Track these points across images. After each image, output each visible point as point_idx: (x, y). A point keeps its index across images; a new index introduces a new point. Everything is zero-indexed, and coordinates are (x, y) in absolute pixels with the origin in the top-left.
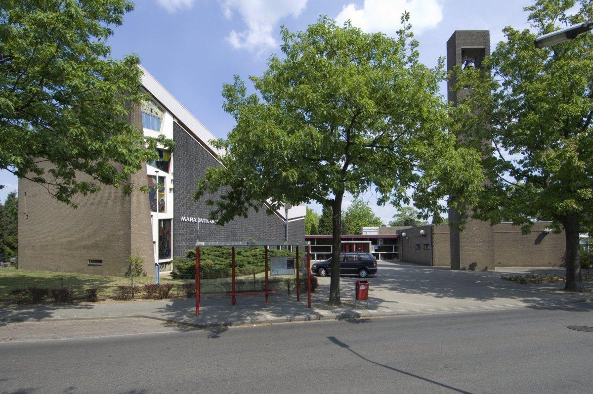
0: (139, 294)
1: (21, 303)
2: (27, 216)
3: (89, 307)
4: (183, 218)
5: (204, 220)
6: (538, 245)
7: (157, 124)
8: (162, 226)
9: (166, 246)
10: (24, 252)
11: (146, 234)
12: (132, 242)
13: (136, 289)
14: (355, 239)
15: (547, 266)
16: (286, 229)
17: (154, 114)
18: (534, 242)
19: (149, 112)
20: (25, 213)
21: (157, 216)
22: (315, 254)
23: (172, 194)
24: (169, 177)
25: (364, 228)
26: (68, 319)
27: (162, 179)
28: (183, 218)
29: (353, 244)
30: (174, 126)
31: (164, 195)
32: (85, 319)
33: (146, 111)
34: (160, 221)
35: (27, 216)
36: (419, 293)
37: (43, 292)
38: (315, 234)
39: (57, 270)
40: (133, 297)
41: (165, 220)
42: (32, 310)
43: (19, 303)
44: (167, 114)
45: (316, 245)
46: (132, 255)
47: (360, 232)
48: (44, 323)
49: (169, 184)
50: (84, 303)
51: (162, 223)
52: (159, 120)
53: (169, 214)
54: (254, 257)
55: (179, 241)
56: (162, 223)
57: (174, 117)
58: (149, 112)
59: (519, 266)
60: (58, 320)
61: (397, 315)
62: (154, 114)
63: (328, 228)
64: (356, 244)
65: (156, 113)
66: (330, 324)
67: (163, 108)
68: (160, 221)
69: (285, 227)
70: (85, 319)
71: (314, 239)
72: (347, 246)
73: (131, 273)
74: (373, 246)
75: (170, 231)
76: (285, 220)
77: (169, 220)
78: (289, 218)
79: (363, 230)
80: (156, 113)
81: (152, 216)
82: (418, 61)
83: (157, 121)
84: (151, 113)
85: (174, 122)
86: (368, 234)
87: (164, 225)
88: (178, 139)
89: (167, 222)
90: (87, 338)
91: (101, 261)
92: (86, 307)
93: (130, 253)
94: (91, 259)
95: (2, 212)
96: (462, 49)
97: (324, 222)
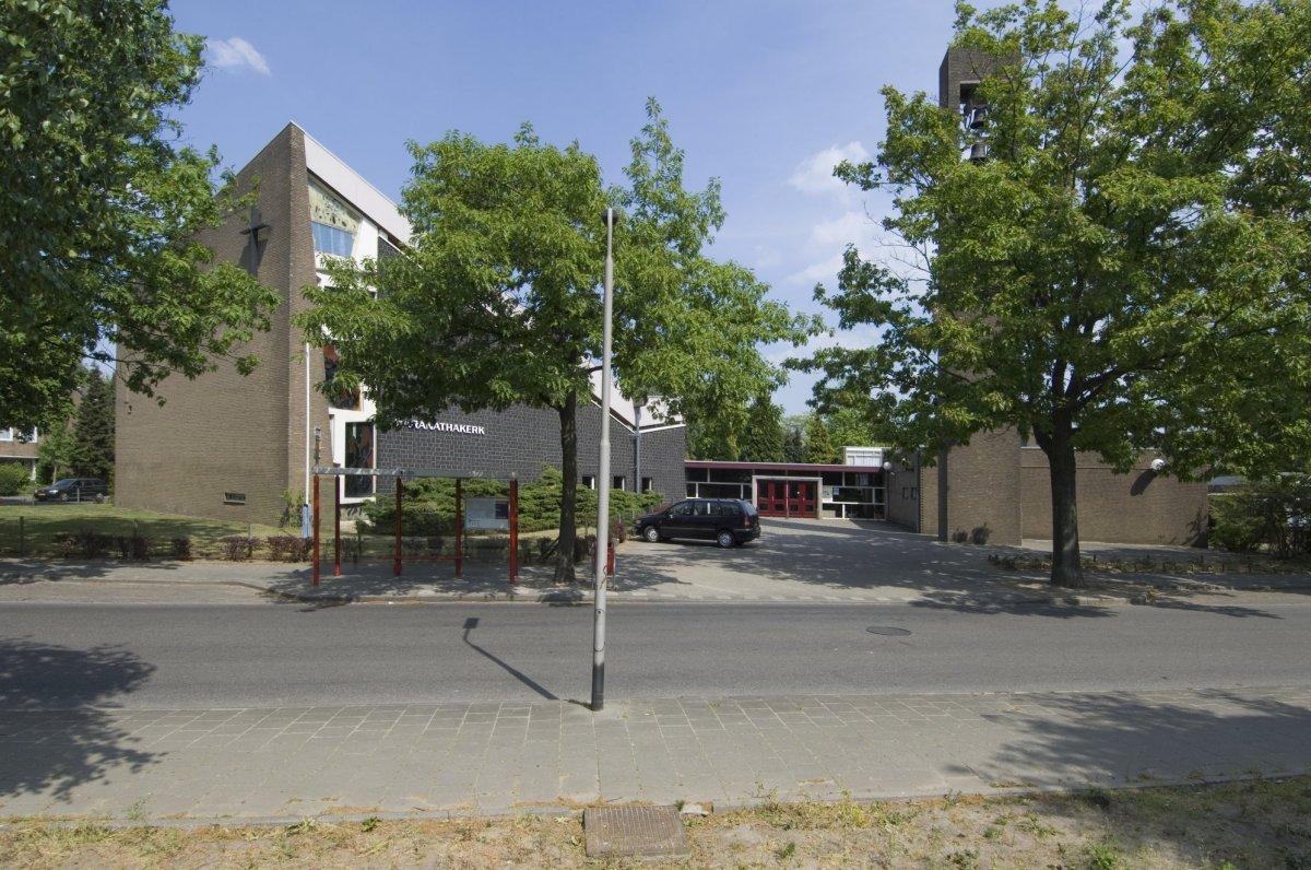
0: (260, 552)
1: (69, 556)
2: (130, 407)
6: (1138, 497)
8: (354, 435)
10: (124, 476)
12: (291, 463)
13: (253, 544)
14: (792, 473)
15: (1154, 542)
16: (635, 447)
17: (339, 224)
18: (1129, 490)
19: (329, 222)
20: (126, 403)
25: (848, 449)
26: (124, 581)
29: (784, 482)
32: (149, 582)
33: (322, 221)
34: (349, 426)
35: (130, 407)
36: (839, 587)
37: (106, 542)
38: (728, 459)
39: (176, 511)
40: (249, 556)
41: (359, 425)
42: (83, 567)
43: (67, 556)
44: (365, 224)
45: (697, 483)
46: (290, 487)
47: (839, 457)
48: (91, 584)
50: (166, 563)
51: (354, 429)
52: (350, 235)
54: (538, 502)
56: (354, 429)
57: (380, 228)
58: (329, 222)
59: (1098, 540)
60: (110, 581)
61: (650, 601)
62: (339, 224)
63: (762, 447)
64: (794, 485)
65: (344, 224)
66: (535, 607)
67: (357, 214)
68: (349, 426)
69: (635, 442)
70: (149, 582)
72: (772, 488)
73: (288, 519)
74: (830, 489)
75: (370, 444)
76: (635, 428)
78: (641, 424)
79: (847, 454)
80: (344, 224)
81: (331, 417)
83: (346, 237)
85: (380, 240)
86: (859, 463)
87: (358, 433)
89: (366, 428)
90: (131, 603)
91: (242, 497)
92: (167, 568)
93: (286, 484)
94: (228, 491)
96: (962, 85)
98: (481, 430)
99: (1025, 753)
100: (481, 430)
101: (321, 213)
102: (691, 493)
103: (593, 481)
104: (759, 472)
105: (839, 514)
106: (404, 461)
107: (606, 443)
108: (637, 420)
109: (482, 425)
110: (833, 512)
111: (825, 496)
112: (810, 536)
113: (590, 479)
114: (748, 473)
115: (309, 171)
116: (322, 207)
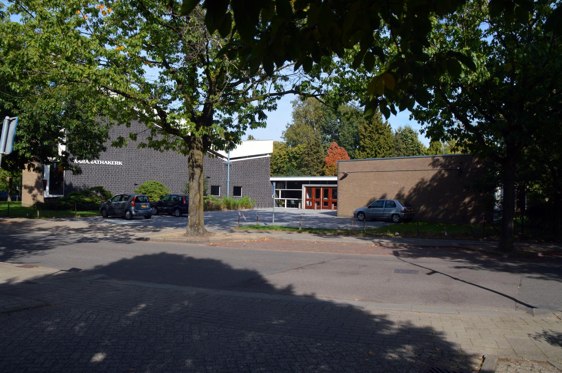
98: (120, 163)
100: (120, 163)
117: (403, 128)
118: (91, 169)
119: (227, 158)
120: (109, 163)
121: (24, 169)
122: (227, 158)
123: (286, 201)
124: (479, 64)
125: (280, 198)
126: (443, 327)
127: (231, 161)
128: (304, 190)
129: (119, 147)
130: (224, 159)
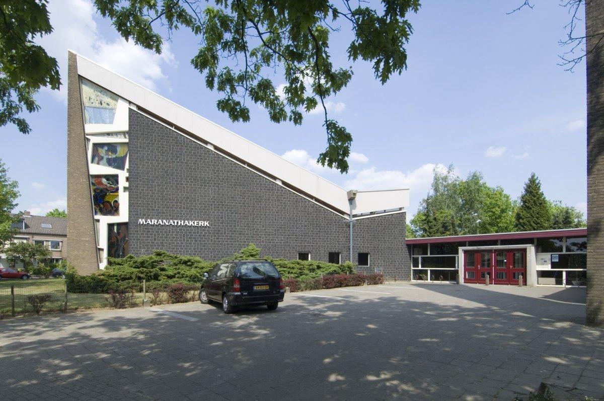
3: (46, 344)
4: (141, 221)
5: (176, 221)
7: (108, 114)
9: (121, 254)
11: (87, 241)
17: (104, 105)
19: (98, 105)
21: (105, 220)
22: (427, 270)
23: (127, 194)
24: (123, 175)
27: (114, 179)
28: (141, 221)
30: (130, 117)
31: (118, 195)
34: (111, 226)
41: (119, 225)
42: (188, 374)
44: (120, 101)
45: (429, 255)
49: (123, 183)
51: (115, 227)
52: (112, 110)
53: (123, 216)
55: (137, 248)
56: (115, 227)
58: (98, 105)
64: (499, 252)
65: (108, 104)
68: (111, 226)
71: (426, 244)
77: (125, 224)
78: (354, 212)
80: (108, 104)
81: (98, 221)
82: (407, 20)
84: (100, 105)
85: (130, 110)
88: (135, 128)
95: (118, 2)
97: (521, 218)
98: (206, 224)
99: (55, 327)
100: (206, 224)
101: (92, 101)
102: (416, 265)
103: (309, 256)
104: (463, 244)
105: (559, 282)
106: (147, 245)
107: (582, 270)
108: (351, 211)
109: (208, 220)
110: (553, 280)
111: (537, 262)
112: (413, 274)
113: (308, 254)
114: (453, 247)
115: (79, 76)
116: (93, 97)
117: (525, 186)
118: (166, 232)
119: (349, 215)
120: (191, 223)
121: (146, 336)
122: (349, 215)
123: (429, 272)
124: (179, 224)
125: (420, 268)
126: (9, 168)
127: (353, 219)
128: (461, 257)
129: (340, 170)
130: (346, 217)
